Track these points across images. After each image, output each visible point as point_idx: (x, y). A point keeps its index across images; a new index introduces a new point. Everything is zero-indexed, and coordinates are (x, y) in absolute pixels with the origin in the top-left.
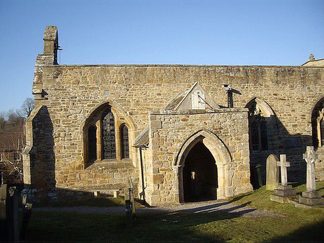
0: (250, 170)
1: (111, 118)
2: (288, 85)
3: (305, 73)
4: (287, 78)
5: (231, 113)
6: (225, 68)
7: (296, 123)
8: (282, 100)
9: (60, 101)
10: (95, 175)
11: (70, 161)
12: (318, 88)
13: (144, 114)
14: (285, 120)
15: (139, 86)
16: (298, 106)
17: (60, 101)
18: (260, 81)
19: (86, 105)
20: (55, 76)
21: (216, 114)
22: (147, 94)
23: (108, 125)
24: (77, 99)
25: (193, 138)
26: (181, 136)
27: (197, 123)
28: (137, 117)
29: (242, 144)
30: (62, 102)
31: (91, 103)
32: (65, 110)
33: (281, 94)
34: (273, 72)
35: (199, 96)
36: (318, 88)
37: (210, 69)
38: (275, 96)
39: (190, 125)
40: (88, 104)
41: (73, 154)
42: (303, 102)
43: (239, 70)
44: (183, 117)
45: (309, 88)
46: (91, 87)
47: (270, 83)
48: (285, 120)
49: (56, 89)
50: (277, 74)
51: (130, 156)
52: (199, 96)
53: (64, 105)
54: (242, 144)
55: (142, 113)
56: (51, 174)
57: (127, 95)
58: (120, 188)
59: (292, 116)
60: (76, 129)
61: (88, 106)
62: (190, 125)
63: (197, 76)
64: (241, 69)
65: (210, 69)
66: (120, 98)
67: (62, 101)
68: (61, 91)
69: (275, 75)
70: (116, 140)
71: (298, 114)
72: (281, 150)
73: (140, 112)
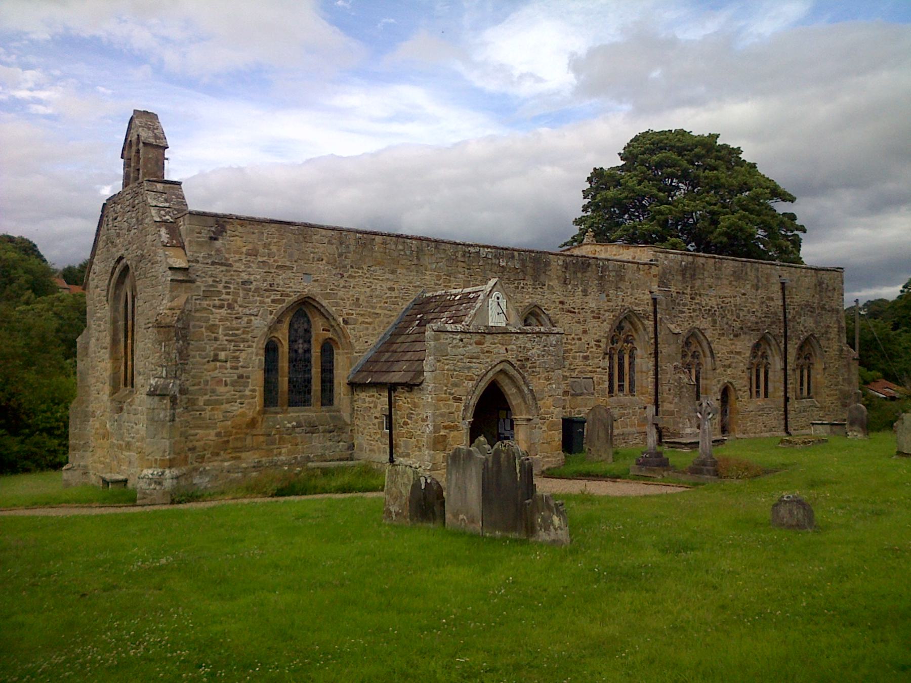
0: (563, 429)
1: (306, 326)
2: (581, 288)
3: (604, 269)
4: (579, 275)
5: (541, 335)
6: (493, 251)
7: (588, 354)
8: (571, 312)
9: (220, 287)
10: (280, 438)
11: (236, 408)
12: (621, 297)
13: (367, 323)
14: (573, 347)
15: (360, 271)
16: (592, 324)
17: (220, 287)
18: (542, 277)
19: (269, 300)
20: (212, 235)
21: (521, 336)
22: (373, 287)
23: (301, 341)
24: (253, 287)
25: (491, 374)
26: (478, 369)
27: (499, 351)
28: (354, 329)
29: (554, 386)
30: (224, 291)
31: (279, 297)
32: (230, 307)
33: (570, 303)
34: (561, 263)
35: (499, 304)
36: (621, 297)
37: (472, 250)
38: (561, 306)
39: (487, 352)
40: (272, 297)
41: (241, 397)
42: (599, 318)
43: (513, 257)
44: (478, 337)
45: (608, 296)
46: (280, 264)
47: (555, 283)
48: (573, 347)
49: (213, 263)
50: (566, 268)
51: (336, 402)
52: (499, 304)
53: (228, 297)
54: (554, 386)
55: (363, 322)
56: (198, 437)
57: (341, 286)
58: (897, 427)
59: (583, 341)
60: (249, 347)
61: (273, 301)
62: (487, 352)
63: (452, 260)
64: (516, 253)
65: (472, 250)
66: (328, 291)
67: (225, 287)
68: (224, 268)
69: (564, 270)
70: (313, 371)
71: (590, 338)
72: (566, 398)
73: (361, 319)
